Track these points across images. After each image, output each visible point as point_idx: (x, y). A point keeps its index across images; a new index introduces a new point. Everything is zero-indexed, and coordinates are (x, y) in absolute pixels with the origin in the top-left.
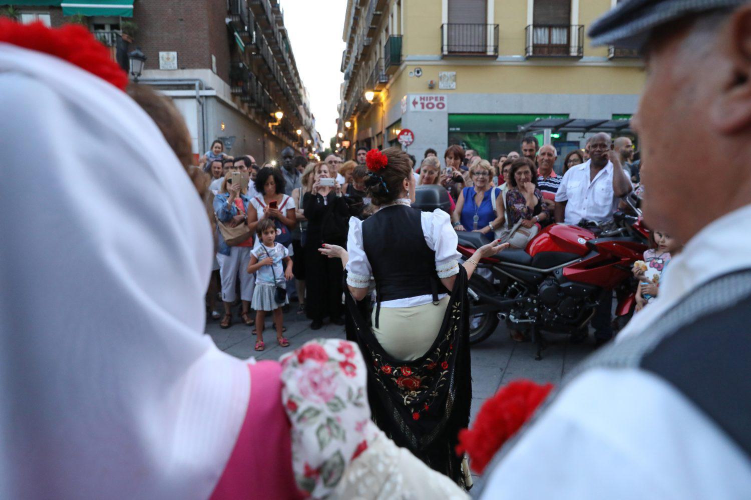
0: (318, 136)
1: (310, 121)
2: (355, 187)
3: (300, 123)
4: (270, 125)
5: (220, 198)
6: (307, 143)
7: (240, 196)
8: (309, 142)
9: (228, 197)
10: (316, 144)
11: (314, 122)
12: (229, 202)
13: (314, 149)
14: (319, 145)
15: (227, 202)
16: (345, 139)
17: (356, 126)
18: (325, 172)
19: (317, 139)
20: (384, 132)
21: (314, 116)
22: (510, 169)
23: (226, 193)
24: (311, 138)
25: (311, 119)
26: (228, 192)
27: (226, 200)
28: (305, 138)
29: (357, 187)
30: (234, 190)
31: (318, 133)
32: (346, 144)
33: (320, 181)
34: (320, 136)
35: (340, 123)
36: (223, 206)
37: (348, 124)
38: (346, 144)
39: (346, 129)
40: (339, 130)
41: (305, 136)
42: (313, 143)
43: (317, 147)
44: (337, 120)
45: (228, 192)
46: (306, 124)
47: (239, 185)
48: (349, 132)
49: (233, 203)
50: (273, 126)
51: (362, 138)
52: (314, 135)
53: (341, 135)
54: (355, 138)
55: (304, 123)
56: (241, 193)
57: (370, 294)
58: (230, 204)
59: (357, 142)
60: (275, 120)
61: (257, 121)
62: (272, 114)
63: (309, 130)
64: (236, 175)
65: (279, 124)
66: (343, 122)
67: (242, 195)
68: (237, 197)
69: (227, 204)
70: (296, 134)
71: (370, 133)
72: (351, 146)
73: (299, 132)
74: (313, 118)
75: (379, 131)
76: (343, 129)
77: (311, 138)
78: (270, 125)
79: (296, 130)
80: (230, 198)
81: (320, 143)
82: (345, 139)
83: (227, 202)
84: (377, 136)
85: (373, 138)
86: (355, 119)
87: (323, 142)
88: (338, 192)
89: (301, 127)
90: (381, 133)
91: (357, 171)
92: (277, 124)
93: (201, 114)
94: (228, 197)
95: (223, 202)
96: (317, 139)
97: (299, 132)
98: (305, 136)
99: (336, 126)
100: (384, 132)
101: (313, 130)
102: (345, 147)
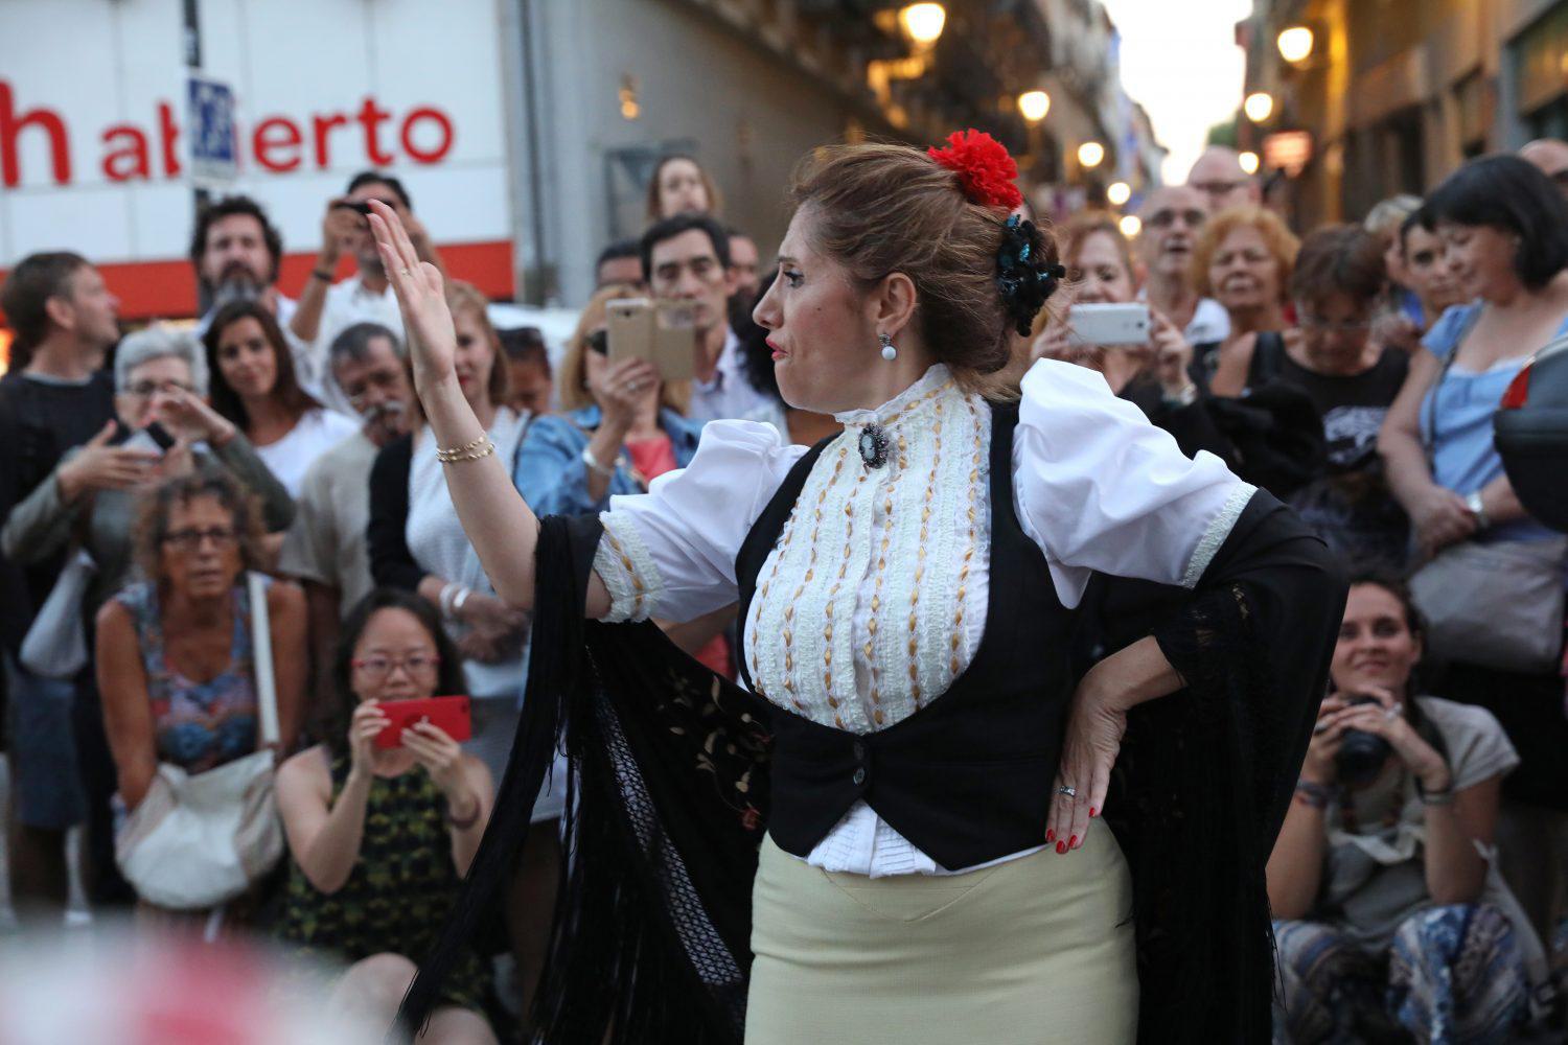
0: (1141, 127)
1: (1091, 43)
2: (1298, 353)
3: (1035, 57)
4: (878, 76)
5: (552, 437)
6: (1080, 168)
7: (661, 424)
8: (1090, 155)
9: (594, 429)
10: (1127, 162)
11: (1116, 48)
12: (599, 457)
13: (1118, 193)
14: (1145, 172)
15: (588, 456)
16: (1282, 123)
17: (1338, 47)
18: (1105, 274)
19: (1132, 137)
20: (1495, 63)
21: (1114, 18)
22: (150, 597)
23: (585, 411)
24: (1102, 135)
25: (1098, 32)
26: (593, 401)
27: (581, 448)
28: (1065, 137)
29: (1315, 349)
30: (620, 394)
31: (1138, 107)
32: (1290, 150)
33: (1070, 323)
34: (1146, 119)
35: (1255, 39)
36: (566, 477)
37: (1295, 44)
38: (1290, 150)
39: (1287, 70)
40: (1252, 84)
41: (1068, 126)
42: (1110, 161)
43: (1136, 180)
44: (1240, 30)
45: (593, 401)
46: (1070, 62)
47: (646, 367)
48: (1300, 98)
49: (621, 461)
50: (893, 82)
51: (1373, 109)
52: (1115, 119)
53: (1261, 108)
54: (1335, 117)
55: (1058, 56)
56: (665, 403)
57: (1377, 948)
58: (601, 468)
59: (1350, 139)
60: (900, 46)
61: (808, 60)
62: (885, 20)
63: (1087, 96)
64: (627, 313)
65: (927, 73)
66: (1267, 34)
67: (671, 417)
68: (639, 429)
69: (587, 467)
70: (1017, 116)
71: (1416, 78)
72: (1312, 165)
73: (1034, 106)
74: (1110, 28)
75: (1465, 60)
76: (1270, 73)
77: (1102, 135)
78: (878, 76)
79: (1016, 95)
80: (600, 438)
81: (1152, 158)
82: (1282, 123)
83: (588, 456)
84: (1460, 87)
85: (1435, 104)
86: (1334, 14)
87: (1165, 151)
88: (1174, 379)
89: (1049, 80)
90: (1477, 71)
91: (1325, 261)
92: (912, 68)
93: (515, 32)
94: (594, 429)
95: (569, 456)
96: (1132, 137)
97: (1034, 106)
98: (1068, 126)
99: (1238, 58)
100: (1495, 63)
101: (1111, 90)
102: (1281, 170)
